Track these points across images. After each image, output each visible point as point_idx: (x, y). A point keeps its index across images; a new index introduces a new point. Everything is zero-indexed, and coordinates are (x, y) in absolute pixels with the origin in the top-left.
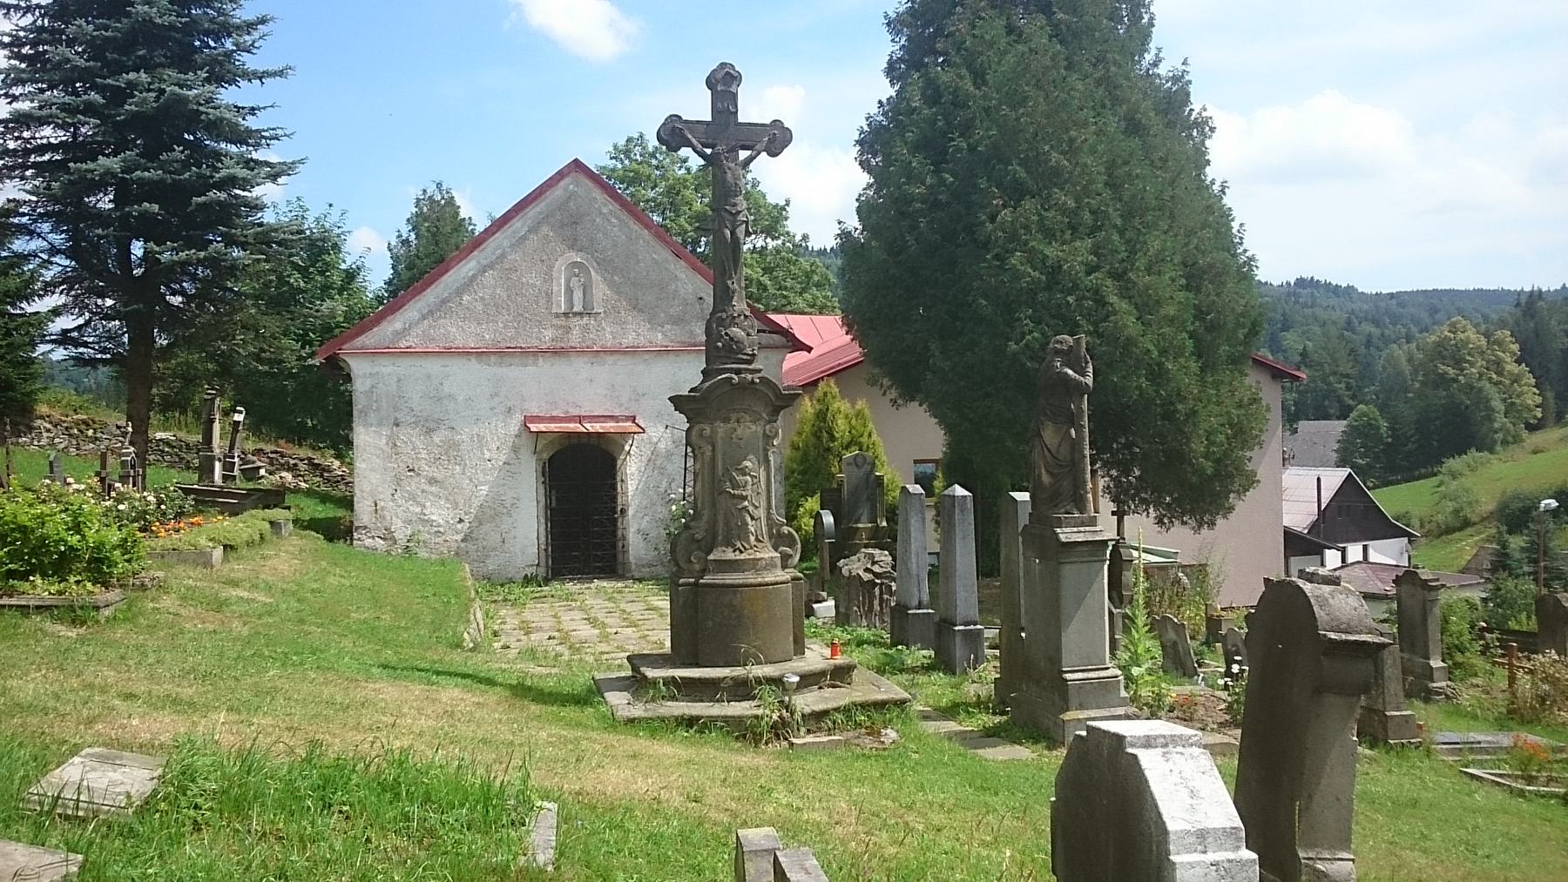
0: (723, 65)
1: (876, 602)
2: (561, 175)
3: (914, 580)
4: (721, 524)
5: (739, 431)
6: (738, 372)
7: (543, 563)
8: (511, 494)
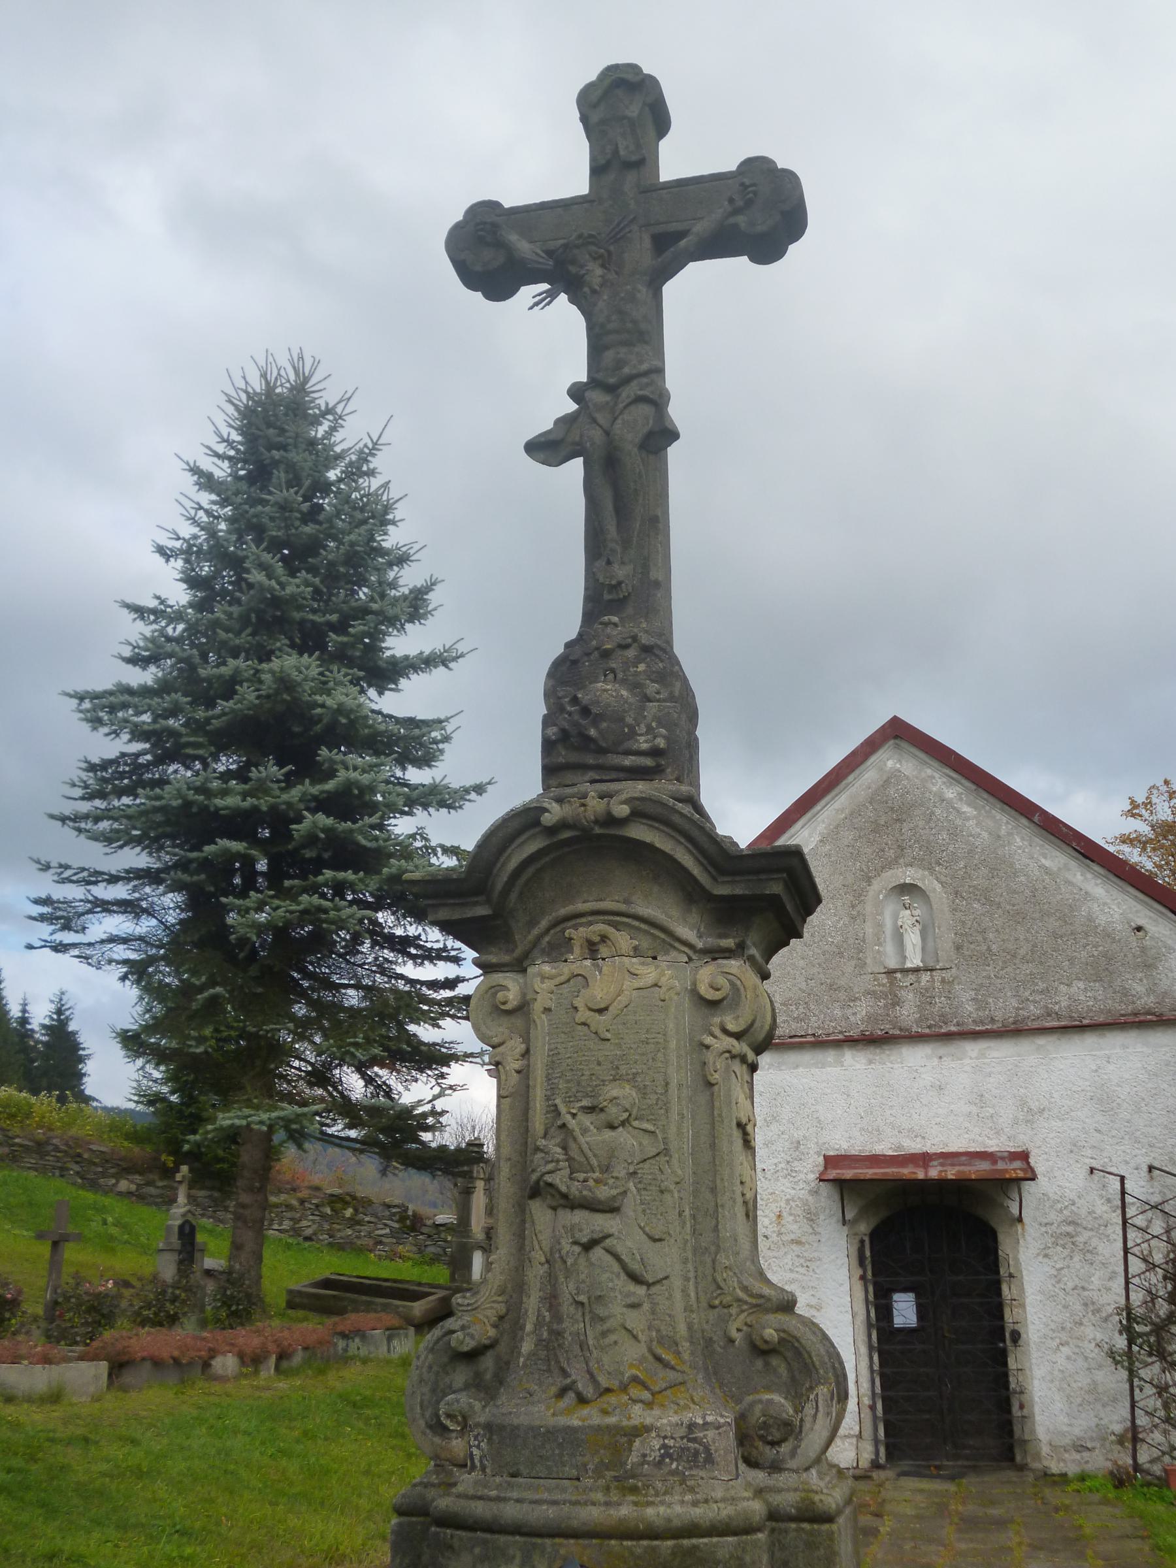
2: (870, 746)
4: (532, 1303)
7: (868, 1433)
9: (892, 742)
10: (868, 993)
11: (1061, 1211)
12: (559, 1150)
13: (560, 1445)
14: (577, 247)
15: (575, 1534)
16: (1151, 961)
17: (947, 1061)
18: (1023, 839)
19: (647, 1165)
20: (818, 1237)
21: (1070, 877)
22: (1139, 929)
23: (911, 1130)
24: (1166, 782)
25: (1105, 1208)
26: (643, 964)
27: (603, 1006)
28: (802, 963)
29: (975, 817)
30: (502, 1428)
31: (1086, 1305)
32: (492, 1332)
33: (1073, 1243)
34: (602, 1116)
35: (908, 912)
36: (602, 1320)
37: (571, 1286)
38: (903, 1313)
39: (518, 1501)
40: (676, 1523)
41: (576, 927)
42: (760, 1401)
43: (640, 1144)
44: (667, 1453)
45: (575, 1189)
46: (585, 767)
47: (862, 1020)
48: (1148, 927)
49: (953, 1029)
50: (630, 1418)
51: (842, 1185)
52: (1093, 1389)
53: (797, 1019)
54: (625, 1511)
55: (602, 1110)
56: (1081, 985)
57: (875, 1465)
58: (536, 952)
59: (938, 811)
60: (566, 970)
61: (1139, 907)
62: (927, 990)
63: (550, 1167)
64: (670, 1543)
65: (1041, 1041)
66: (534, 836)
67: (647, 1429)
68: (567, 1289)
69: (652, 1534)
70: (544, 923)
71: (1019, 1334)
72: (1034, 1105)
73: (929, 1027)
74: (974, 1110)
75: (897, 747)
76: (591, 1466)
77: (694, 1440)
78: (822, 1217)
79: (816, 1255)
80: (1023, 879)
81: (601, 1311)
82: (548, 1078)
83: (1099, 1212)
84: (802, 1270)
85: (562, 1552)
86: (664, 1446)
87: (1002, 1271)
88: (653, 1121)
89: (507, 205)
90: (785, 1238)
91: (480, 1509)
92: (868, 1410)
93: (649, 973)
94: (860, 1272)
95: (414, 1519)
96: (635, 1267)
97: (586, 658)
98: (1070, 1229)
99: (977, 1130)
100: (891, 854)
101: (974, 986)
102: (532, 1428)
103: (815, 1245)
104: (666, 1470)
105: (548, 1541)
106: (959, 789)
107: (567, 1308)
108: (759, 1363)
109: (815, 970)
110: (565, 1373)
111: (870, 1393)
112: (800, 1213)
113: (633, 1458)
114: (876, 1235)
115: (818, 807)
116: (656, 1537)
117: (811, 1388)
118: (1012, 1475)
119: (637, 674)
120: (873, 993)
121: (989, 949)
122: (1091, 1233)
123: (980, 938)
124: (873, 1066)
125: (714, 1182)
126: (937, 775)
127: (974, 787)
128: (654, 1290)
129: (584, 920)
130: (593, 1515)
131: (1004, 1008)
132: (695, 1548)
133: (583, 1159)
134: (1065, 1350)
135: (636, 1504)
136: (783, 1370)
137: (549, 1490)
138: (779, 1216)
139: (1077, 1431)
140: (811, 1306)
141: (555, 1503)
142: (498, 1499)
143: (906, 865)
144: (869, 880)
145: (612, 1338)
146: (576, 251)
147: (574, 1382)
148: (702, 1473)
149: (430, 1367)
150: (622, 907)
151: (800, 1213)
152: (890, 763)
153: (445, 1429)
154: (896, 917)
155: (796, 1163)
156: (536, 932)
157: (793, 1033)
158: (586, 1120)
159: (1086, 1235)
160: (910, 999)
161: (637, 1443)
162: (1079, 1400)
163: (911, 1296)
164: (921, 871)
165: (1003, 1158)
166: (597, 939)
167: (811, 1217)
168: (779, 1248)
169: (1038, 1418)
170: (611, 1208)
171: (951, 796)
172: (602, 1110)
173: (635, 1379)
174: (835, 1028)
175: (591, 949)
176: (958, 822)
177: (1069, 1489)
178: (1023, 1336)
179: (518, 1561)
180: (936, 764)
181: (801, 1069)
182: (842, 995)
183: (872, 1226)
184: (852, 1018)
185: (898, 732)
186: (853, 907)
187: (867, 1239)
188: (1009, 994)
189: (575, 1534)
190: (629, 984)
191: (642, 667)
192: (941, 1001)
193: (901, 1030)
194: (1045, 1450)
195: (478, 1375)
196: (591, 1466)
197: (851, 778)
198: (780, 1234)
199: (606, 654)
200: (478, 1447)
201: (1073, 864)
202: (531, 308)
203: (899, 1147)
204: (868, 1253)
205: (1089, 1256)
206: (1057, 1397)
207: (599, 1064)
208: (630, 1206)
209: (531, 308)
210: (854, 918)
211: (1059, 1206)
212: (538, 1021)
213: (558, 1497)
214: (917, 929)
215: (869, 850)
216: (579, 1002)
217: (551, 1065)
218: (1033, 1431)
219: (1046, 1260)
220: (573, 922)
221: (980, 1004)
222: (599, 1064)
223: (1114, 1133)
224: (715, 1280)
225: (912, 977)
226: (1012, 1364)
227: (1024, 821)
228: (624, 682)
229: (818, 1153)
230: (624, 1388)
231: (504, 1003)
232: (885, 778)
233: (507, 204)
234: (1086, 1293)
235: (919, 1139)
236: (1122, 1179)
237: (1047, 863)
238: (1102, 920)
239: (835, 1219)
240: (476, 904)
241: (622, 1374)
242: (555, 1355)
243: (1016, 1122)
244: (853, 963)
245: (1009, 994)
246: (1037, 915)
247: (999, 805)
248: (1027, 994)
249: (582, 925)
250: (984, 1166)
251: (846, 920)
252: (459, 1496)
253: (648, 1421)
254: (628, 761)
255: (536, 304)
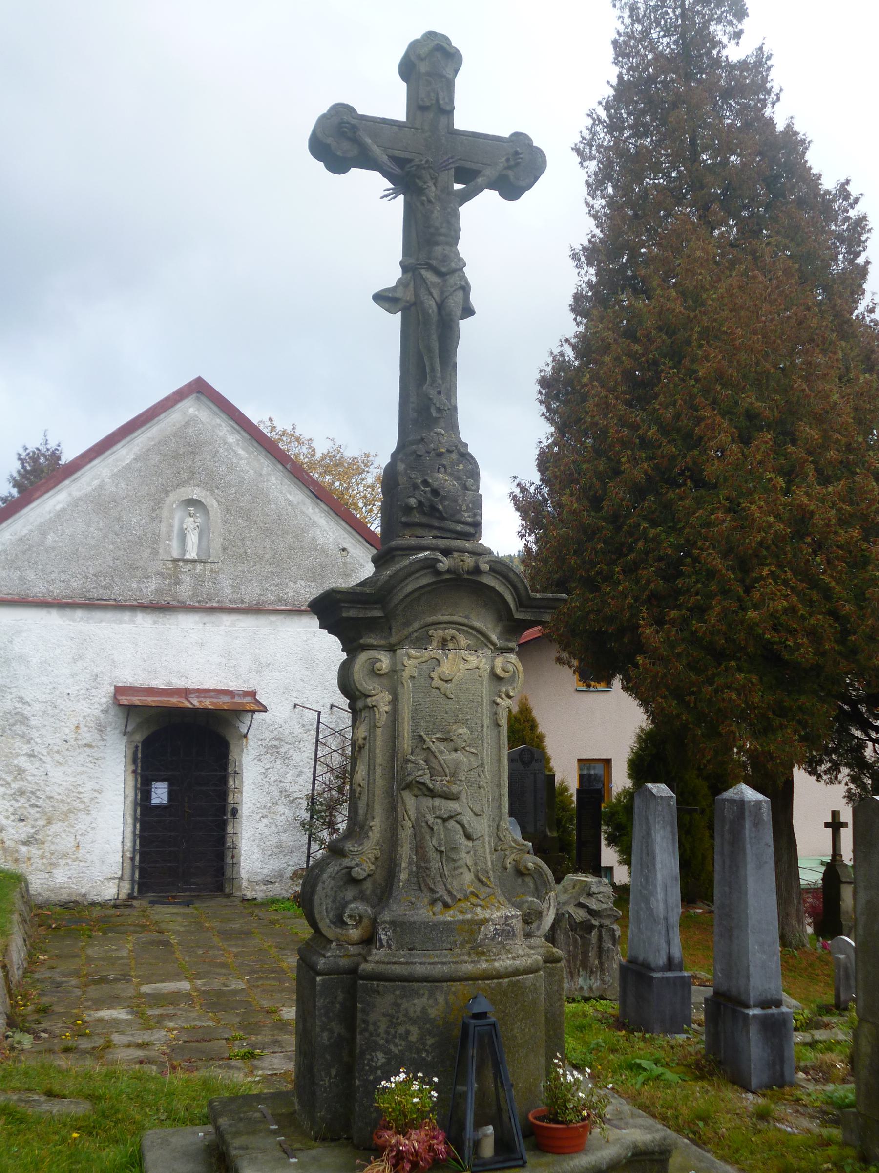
0: (431, 35)
1: (592, 954)
2: (179, 396)
3: (662, 928)
4: (405, 851)
5: (446, 668)
6: (447, 552)
7: (127, 876)
8: (90, 785)
9: (195, 395)
10: (158, 573)
11: (272, 731)
12: (422, 762)
13: (441, 932)
14: (424, 168)
15: (460, 980)
16: (348, 572)
17: (208, 627)
18: (277, 479)
19: (472, 773)
20: (104, 743)
21: (304, 510)
22: (344, 550)
23: (178, 672)
24: (270, 420)
25: (300, 730)
26: (470, 654)
27: (450, 678)
28: (111, 547)
29: (246, 458)
30: (402, 924)
31: (281, 792)
32: (373, 867)
33: (278, 752)
34: (452, 744)
35: (192, 519)
36: (454, 860)
37: (434, 842)
38: (161, 796)
39: (421, 963)
40: (510, 969)
41: (435, 630)
42: (527, 902)
43: (469, 760)
44: (497, 933)
45: (438, 787)
46: (430, 527)
47: (151, 592)
48: (350, 549)
49: (215, 604)
50: (477, 915)
51: (129, 710)
52: (279, 845)
53: (104, 587)
54: (484, 965)
55: (452, 741)
56: (303, 583)
57: (131, 897)
58: (407, 642)
59: (221, 450)
60: (426, 654)
61: (346, 535)
62: (200, 576)
63: (420, 772)
64: (507, 980)
65: (273, 618)
66: (425, 575)
67: (487, 920)
68: (431, 843)
69: (499, 976)
70: (416, 625)
71: (237, 810)
72: (263, 661)
73: (199, 602)
74: (224, 661)
75: (198, 399)
76: (458, 942)
77: (508, 925)
78: (109, 729)
79: (101, 755)
80: (273, 506)
81: (454, 856)
82: (413, 719)
83: (296, 733)
84: (91, 765)
85: (453, 989)
86: (495, 929)
87: (230, 770)
88: (476, 747)
89: (360, 112)
90: (80, 743)
91: (397, 969)
92: (129, 861)
93: (473, 660)
94: (133, 768)
95: (332, 976)
96: (470, 830)
97: (427, 455)
98: (277, 743)
99: (223, 675)
100: (185, 476)
101: (232, 577)
102: (424, 923)
103: (102, 748)
104: (496, 942)
105: (445, 984)
106: (238, 437)
107: (432, 854)
108: (520, 881)
109: (121, 553)
110: (432, 891)
111: (131, 849)
112: (93, 725)
113: (481, 937)
114: (147, 743)
115: (135, 434)
116: (500, 978)
117: (547, 893)
118: (224, 901)
119: (458, 471)
120: (161, 574)
121: (245, 552)
122: (289, 746)
123: (240, 544)
124: (156, 625)
125: (499, 781)
126: (224, 425)
127: (249, 437)
128: (476, 842)
129: (441, 626)
130: (468, 968)
131: (251, 593)
132: (518, 981)
133: (441, 769)
134: (265, 821)
135: (487, 961)
136: (531, 885)
137: (437, 956)
138: (77, 727)
139: (266, 872)
140: (95, 791)
141: (444, 963)
142: (407, 963)
143: (195, 486)
144: (167, 493)
145: (461, 870)
146: (423, 172)
147: (441, 896)
148: (511, 942)
149: (332, 888)
150: (465, 621)
151: (93, 725)
152: (191, 410)
153: (346, 924)
154: (182, 522)
155: (93, 690)
156: (411, 629)
157: (100, 597)
158: (442, 746)
159: (287, 747)
160: (187, 582)
161: (483, 929)
162: (269, 852)
163: (165, 785)
164: (204, 492)
165: (239, 695)
166: (449, 638)
167: (101, 729)
168: (75, 749)
169: (242, 864)
170: (454, 797)
171: (231, 441)
172: (452, 741)
173: (472, 893)
174: (131, 596)
175: (444, 644)
176: (235, 460)
177: (271, 909)
178: (240, 812)
179: (426, 996)
180: (224, 416)
181: (103, 624)
182: (139, 573)
183: (144, 737)
184: (144, 591)
185: (200, 389)
186: (154, 510)
187: (140, 745)
188: (255, 584)
189: (460, 980)
190: (463, 666)
191: (461, 467)
192: (208, 585)
193: (179, 602)
194: (245, 884)
195: (362, 892)
196: (458, 942)
197: (162, 416)
198: (76, 739)
199: (440, 455)
200: (386, 934)
201: (308, 501)
202: (382, 198)
203: (170, 683)
204: (140, 755)
205: (287, 761)
206: (256, 851)
207: (446, 713)
208: (463, 797)
209: (382, 198)
210: (153, 519)
211: (272, 728)
212: (405, 684)
213: (444, 960)
214: (197, 532)
215: (169, 471)
216: (434, 675)
217: (415, 711)
218: (238, 872)
219: (259, 763)
220: (435, 626)
221: (235, 589)
222: (446, 713)
223: (312, 682)
224: (498, 836)
225: (190, 566)
226: (230, 830)
227: (280, 467)
228: (451, 474)
229: (111, 684)
230: (467, 898)
231: (379, 670)
232: (186, 420)
233: (360, 111)
234: (282, 785)
235: (183, 679)
236: (319, 713)
237: (291, 498)
238: (321, 541)
239: (118, 731)
240: (376, 609)
241: (466, 891)
242: (424, 881)
243: (250, 671)
244: (149, 551)
245: (255, 584)
246: (280, 533)
247: (264, 452)
248: (267, 585)
249: (439, 629)
250: (226, 699)
251: (148, 519)
252: (377, 963)
253: (487, 916)
254: (459, 528)
255: (386, 196)
